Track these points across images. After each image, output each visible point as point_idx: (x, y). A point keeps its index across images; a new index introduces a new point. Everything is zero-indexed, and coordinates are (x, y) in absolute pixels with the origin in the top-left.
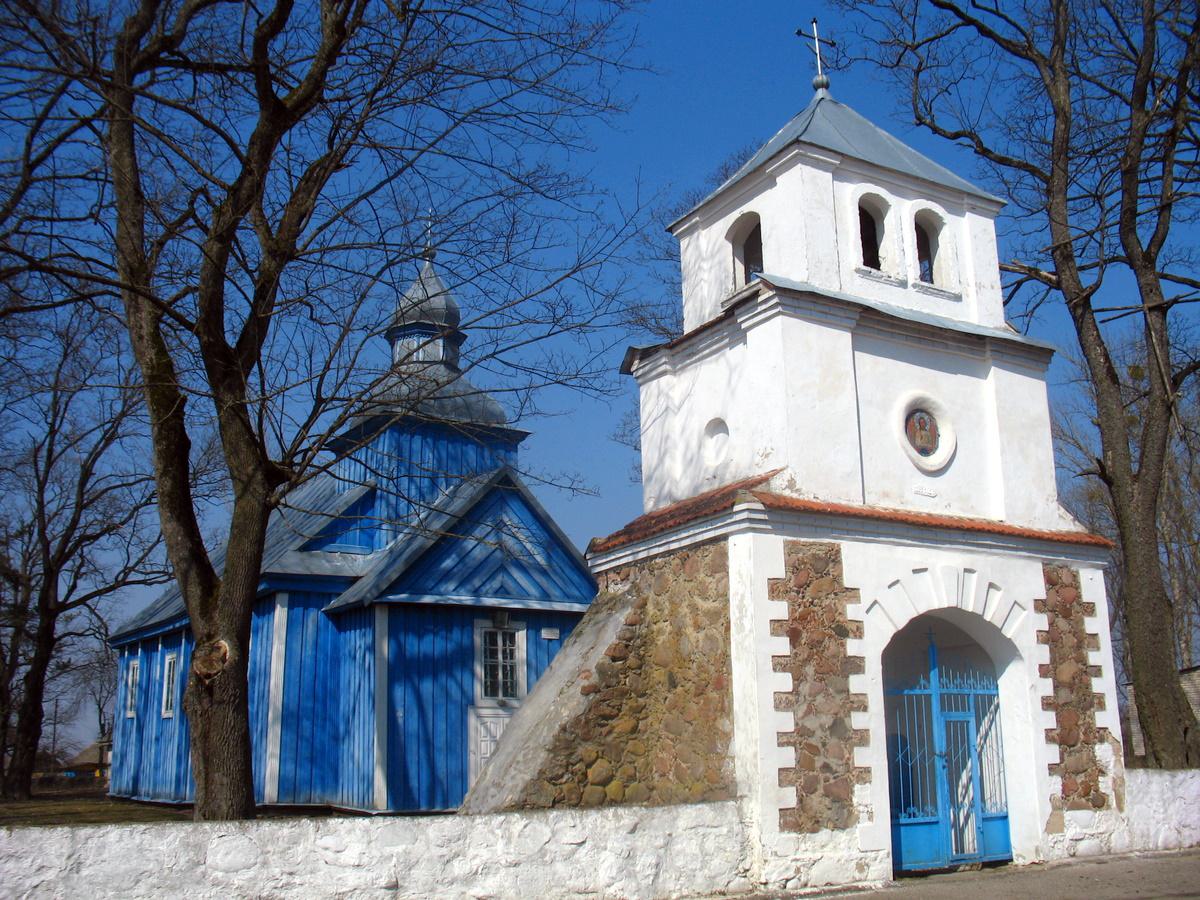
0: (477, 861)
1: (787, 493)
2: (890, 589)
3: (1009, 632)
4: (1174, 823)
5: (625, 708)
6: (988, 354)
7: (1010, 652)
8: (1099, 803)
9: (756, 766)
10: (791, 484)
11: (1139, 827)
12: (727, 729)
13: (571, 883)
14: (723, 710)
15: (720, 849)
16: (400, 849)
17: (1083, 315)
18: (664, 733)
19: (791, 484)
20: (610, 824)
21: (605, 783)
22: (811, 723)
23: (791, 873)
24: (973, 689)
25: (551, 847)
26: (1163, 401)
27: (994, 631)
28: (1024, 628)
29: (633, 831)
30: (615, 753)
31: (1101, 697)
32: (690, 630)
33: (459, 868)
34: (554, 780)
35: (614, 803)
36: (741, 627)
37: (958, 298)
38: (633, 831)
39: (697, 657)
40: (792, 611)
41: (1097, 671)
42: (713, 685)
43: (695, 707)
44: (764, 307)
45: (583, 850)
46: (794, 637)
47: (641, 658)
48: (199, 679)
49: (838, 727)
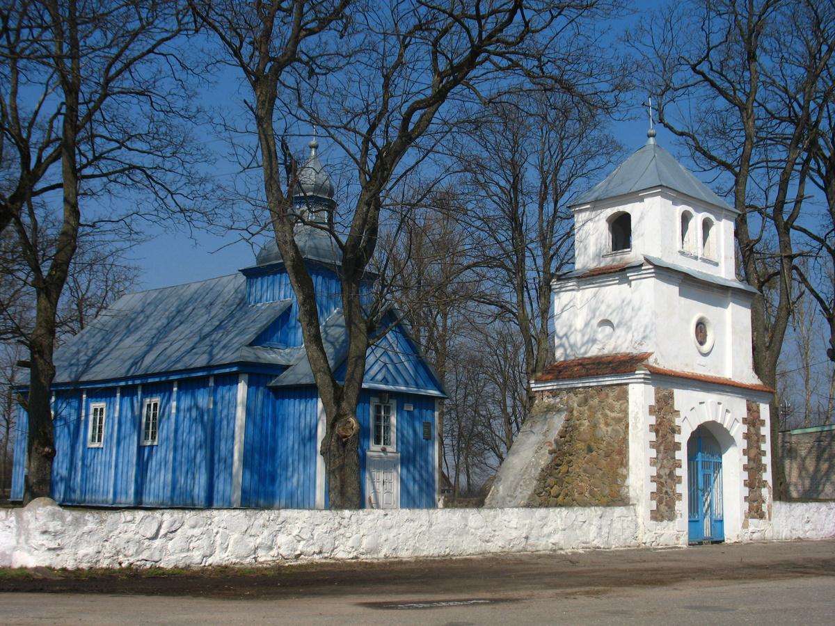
0: (551, 528)
1: (654, 365)
2: (694, 410)
3: (732, 434)
4: (789, 528)
5: (565, 461)
6: (730, 294)
7: (731, 441)
8: (761, 516)
9: (642, 491)
10: (656, 361)
11: (776, 528)
12: (624, 472)
13: (581, 539)
14: (622, 464)
15: (628, 527)
16: (528, 521)
17: (749, 256)
18: (582, 474)
19: (656, 361)
20: (593, 514)
21: (557, 496)
22: (662, 472)
23: (654, 539)
24: (714, 460)
25: (576, 523)
26: (787, 308)
27: (726, 432)
28: (738, 431)
29: (601, 518)
30: (560, 482)
31: (765, 465)
32: (602, 426)
33: (546, 530)
34: (539, 494)
35: (561, 506)
36: (635, 427)
37: (717, 264)
38: (601, 518)
39: (607, 439)
40: (657, 421)
41: (764, 453)
42: (619, 453)
43: (604, 462)
44: (645, 272)
45: (585, 525)
46: (657, 432)
47: (571, 437)
48: (339, 438)
49: (671, 475)
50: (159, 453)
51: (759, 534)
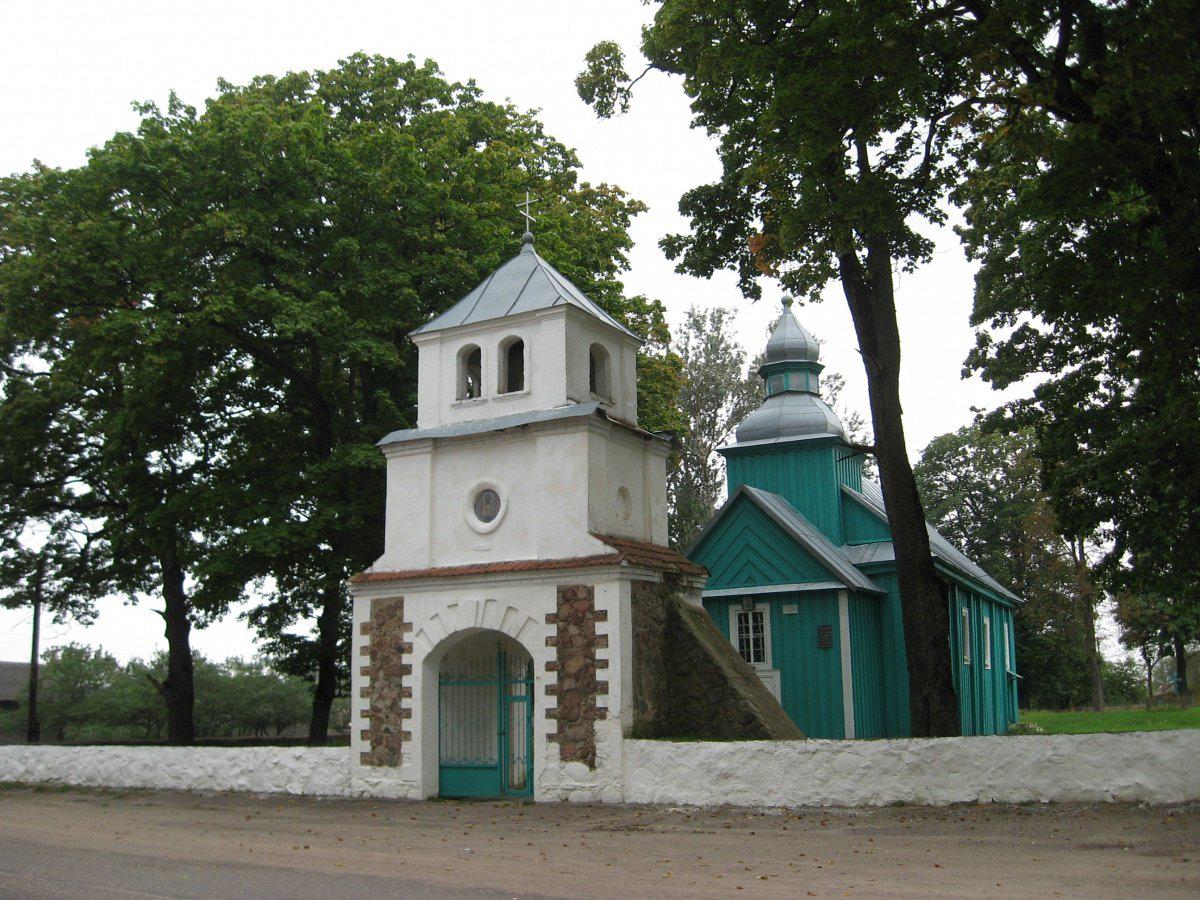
22: (380, 705)
36: (487, 367)
50: (521, 772)
51: (589, 793)
